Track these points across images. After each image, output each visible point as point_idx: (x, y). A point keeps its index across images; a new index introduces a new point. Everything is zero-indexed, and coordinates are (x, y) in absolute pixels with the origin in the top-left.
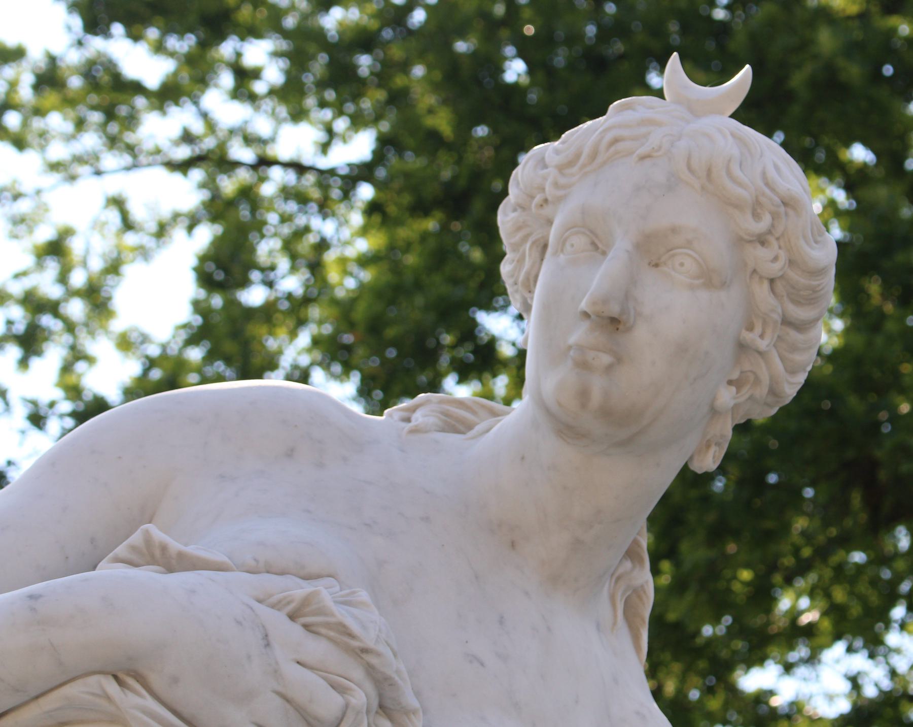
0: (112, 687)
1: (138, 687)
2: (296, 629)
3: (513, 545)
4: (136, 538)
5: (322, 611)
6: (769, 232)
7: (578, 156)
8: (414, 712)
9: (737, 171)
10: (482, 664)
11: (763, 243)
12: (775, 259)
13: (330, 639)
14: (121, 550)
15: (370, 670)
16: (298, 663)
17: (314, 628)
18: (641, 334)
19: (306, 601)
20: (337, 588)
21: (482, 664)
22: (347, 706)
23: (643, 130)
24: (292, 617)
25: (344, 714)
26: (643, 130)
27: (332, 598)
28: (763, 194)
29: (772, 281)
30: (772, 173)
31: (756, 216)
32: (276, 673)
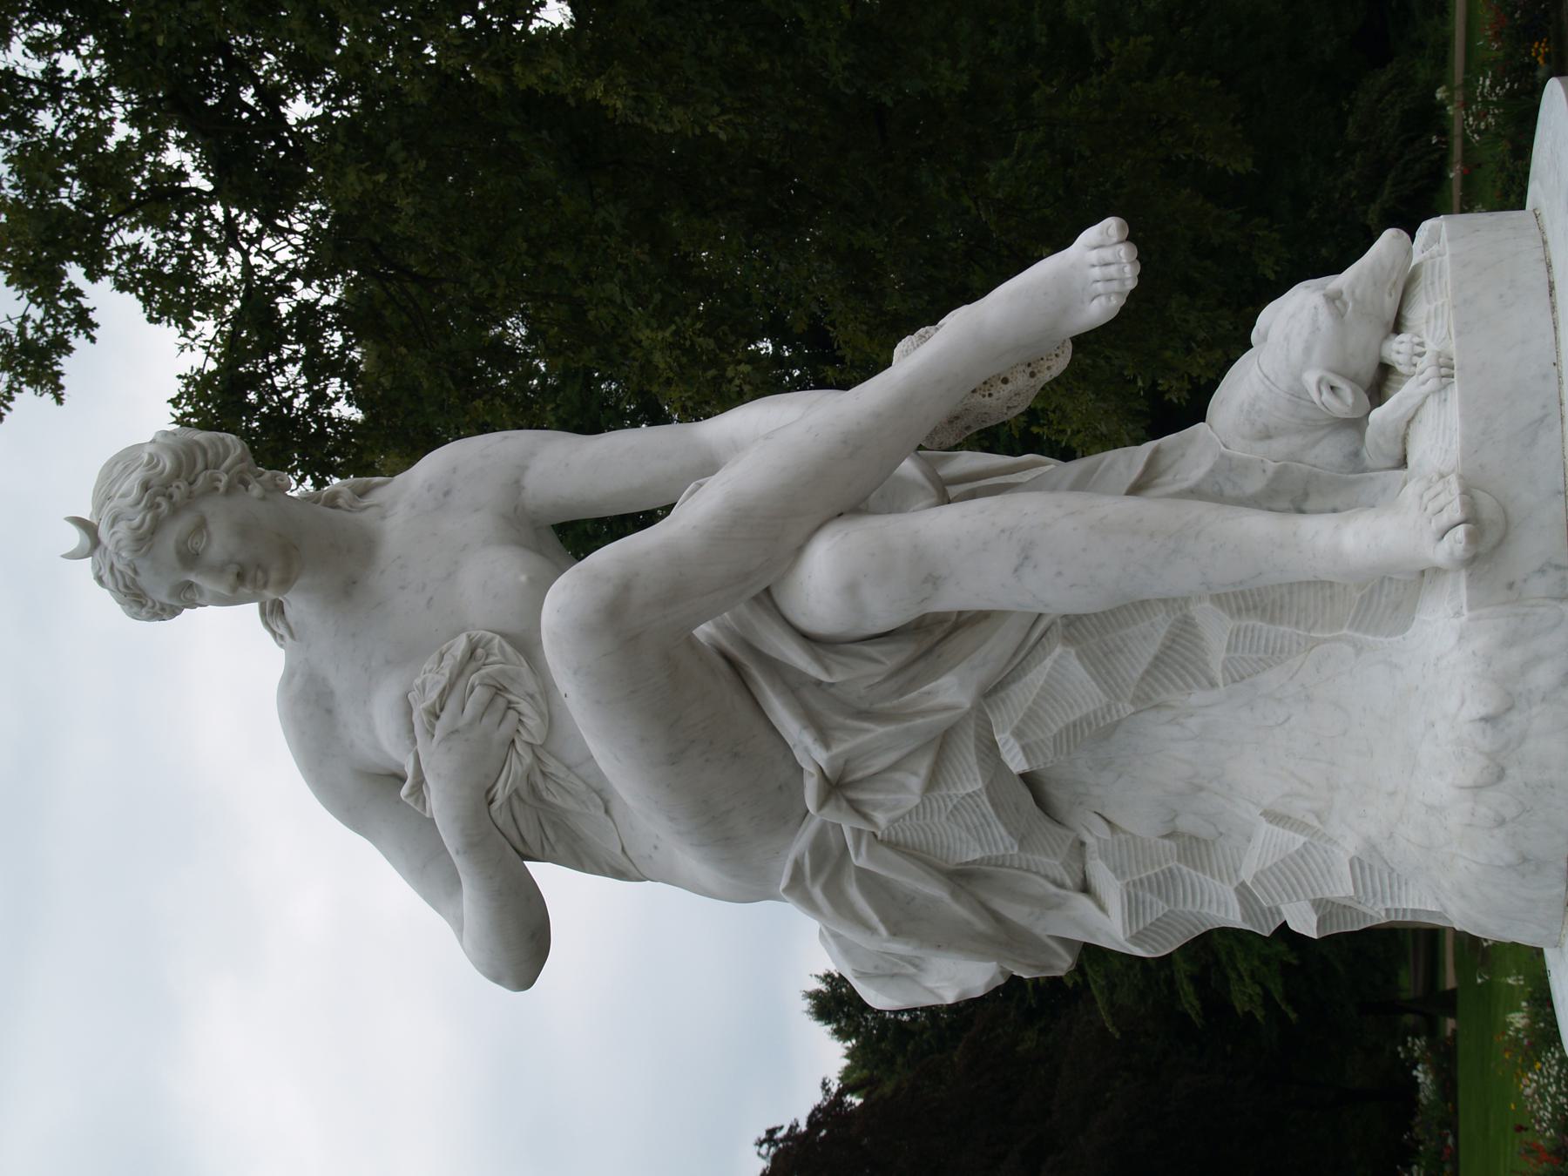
0: (495, 805)
1: (493, 792)
2: (444, 716)
3: (354, 583)
4: (410, 802)
5: (433, 705)
6: (164, 495)
8: (469, 636)
9: (136, 522)
10: (431, 598)
11: (171, 497)
12: (178, 487)
13: (447, 698)
14: (418, 809)
16: (463, 712)
20: (414, 693)
21: (431, 598)
22: (480, 684)
23: (118, 574)
24: (438, 717)
25: (485, 685)
26: (118, 574)
28: (146, 505)
29: (191, 484)
31: (159, 506)
32: (471, 724)
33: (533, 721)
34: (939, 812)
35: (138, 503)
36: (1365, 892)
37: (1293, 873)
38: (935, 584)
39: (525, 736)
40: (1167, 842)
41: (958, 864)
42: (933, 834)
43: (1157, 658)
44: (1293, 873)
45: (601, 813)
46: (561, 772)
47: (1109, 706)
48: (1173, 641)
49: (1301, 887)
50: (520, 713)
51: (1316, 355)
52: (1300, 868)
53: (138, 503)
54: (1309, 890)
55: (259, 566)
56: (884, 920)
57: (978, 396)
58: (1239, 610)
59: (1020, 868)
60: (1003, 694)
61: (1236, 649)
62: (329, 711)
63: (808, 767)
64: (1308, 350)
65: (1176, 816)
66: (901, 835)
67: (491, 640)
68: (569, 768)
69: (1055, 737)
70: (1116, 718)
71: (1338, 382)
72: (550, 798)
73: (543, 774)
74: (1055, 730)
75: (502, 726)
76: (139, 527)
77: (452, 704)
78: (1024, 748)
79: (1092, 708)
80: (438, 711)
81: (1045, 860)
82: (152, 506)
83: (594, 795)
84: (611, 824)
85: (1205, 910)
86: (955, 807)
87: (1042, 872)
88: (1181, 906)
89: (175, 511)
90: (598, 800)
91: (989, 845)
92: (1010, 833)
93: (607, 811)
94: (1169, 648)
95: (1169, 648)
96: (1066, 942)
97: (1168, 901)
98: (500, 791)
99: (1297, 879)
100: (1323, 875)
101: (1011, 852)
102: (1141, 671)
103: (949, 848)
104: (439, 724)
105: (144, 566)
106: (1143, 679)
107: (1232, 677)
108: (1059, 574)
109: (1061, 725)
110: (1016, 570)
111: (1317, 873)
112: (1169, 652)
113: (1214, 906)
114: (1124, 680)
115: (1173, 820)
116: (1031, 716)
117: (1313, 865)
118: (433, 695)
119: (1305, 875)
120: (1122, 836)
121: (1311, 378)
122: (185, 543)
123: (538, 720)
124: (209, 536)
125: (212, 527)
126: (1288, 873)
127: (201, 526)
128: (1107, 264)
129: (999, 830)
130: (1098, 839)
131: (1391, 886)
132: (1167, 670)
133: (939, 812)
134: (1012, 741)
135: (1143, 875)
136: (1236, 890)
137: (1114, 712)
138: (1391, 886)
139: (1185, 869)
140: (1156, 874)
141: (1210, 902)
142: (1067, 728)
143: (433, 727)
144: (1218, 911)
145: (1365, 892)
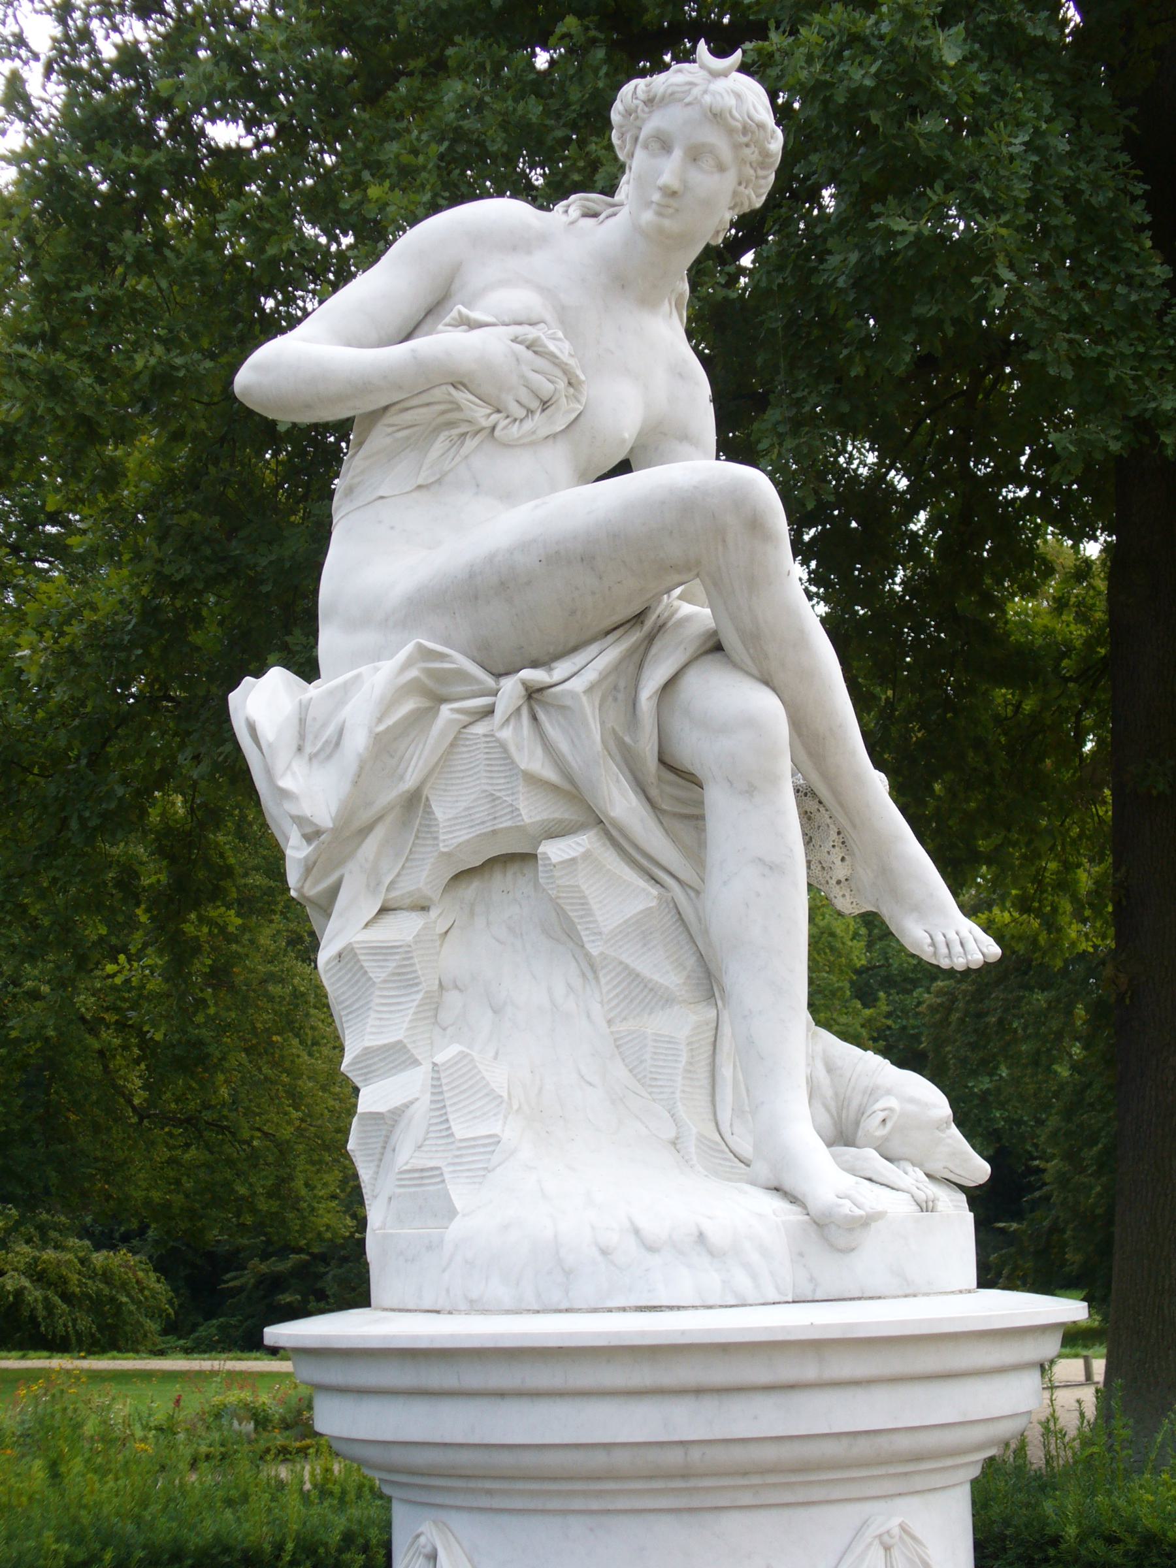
3: (623, 286)
15: (565, 372)
17: (512, 722)
24: (528, 348)
34: (492, 784)
36: (459, 1148)
37: (471, 1087)
38: (747, 792)
40: (437, 982)
41: (427, 799)
42: (463, 778)
43: (638, 975)
44: (471, 1087)
45: (420, 481)
46: (464, 451)
47: (600, 933)
48: (651, 990)
50: (521, 420)
51: (911, 1108)
52: (476, 1092)
53: (752, 120)
54: (455, 1100)
56: (388, 729)
57: (833, 835)
61: (656, 1041)
63: (561, 669)
64: (912, 1100)
65: (461, 991)
66: (465, 749)
67: (579, 401)
69: (578, 886)
71: (889, 1125)
72: (442, 437)
73: (464, 435)
74: (584, 887)
75: (515, 404)
76: (730, 113)
77: (540, 362)
78: (573, 860)
79: (600, 919)
80: (536, 349)
81: (425, 873)
82: (745, 130)
83: (438, 476)
84: (408, 489)
85: (373, 1015)
86: (499, 798)
87: (404, 872)
88: (378, 993)
89: (737, 147)
90: (431, 480)
91: (450, 826)
92: (459, 845)
94: (646, 986)
95: (646, 986)
96: (334, 892)
97: (385, 981)
98: (464, 395)
99: (465, 1091)
100: (470, 1112)
101: (441, 845)
102: (628, 961)
103: (445, 790)
106: (621, 963)
107: (621, 1038)
108: (758, 895)
109: (587, 893)
110: (760, 860)
111: (472, 1108)
112: (642, 985)
113: (377, 1023)
114: (620, 947)
115: (456, 987)
117: (479, 1104)
118: (552, 347)
119: (468, 1097)
120: (438, 943)
121: (892, 1102)
122: (711, 152)
123: (516, 436)
126: (470, 1083)
127: (721, 168)
128: (962, 944)
129: (464, 835)
130: (435, 922)
131: (468, 1170)
132: (625, 984)
133: (492, 784)
134: (582, 850)
135: (416, 960)
136: (400, 1042)
137: (592, 938)
138: (468, 1170)
139: (420, 996)
140: (415, 971)
141: (380, 1019)
142: (584, 897)
143: (520, 343)
144: (373, 1026)
145: (459, 1148)
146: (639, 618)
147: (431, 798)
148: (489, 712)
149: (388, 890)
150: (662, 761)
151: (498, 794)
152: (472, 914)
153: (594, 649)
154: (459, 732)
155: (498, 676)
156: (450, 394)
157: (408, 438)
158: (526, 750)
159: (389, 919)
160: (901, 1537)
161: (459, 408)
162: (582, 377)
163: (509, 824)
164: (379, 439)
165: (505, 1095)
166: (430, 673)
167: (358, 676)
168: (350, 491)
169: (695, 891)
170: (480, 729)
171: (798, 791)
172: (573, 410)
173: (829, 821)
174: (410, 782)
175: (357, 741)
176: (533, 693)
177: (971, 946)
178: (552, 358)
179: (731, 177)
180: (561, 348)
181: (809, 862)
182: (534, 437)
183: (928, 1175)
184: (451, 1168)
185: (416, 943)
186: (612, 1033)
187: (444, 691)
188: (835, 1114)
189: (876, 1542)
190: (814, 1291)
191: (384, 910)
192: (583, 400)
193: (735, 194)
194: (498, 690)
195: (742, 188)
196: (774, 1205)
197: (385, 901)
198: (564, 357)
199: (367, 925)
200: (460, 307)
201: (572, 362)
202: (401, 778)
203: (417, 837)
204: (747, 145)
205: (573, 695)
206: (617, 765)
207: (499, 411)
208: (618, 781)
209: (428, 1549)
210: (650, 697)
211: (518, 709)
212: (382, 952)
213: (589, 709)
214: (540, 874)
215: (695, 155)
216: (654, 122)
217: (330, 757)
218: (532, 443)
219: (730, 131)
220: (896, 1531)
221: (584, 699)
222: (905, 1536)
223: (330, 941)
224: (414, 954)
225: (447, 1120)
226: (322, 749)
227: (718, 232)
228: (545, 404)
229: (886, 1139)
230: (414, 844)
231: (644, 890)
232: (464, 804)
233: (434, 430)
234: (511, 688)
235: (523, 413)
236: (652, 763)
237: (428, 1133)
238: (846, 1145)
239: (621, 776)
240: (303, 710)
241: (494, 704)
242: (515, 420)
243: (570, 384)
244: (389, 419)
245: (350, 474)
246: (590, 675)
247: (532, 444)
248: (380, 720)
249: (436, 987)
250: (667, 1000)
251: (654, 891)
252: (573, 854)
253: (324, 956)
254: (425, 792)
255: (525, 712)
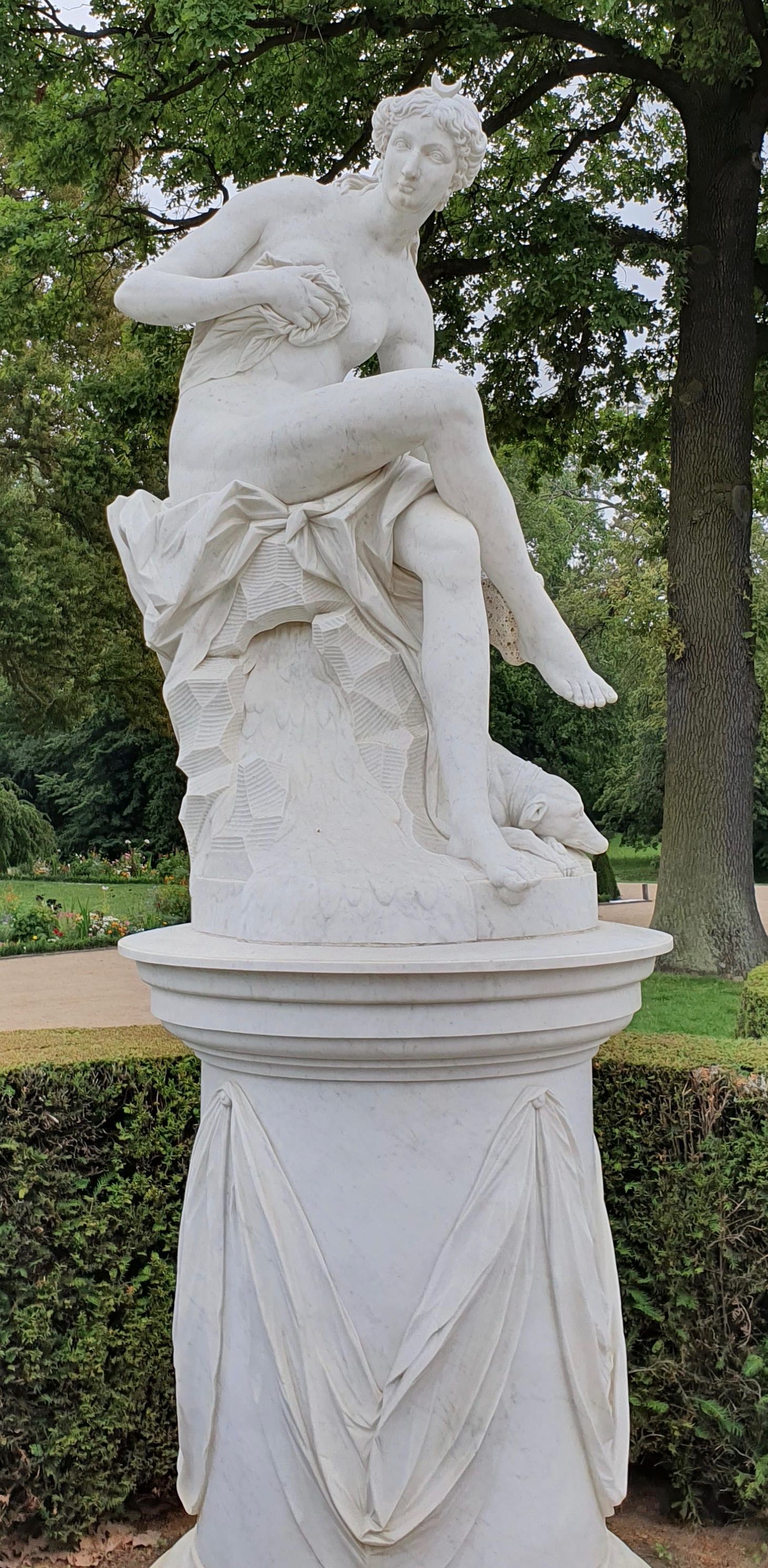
0: (261, 309)
5: (322, 280)
7: (401, 111)
15: (336, 298)
17: (298, 538)
18: (422, 180)
19: (317, 276)
23: (424, 105)
24: (312, 281)
27: (275, 781)
30: (467, 122)
32: (309, 301)
33: (302, 337)
35: (466, 126)
39: (294, 332)
41: (240, 585)
45: (238, 370)
46: (268, 350)
49: (255, 788)
52: (267, 787)
53: (466, 126)
55: (414, 189)
58: (411, 755)
59: (227, 619)
60: (359, 619)
62: (305, 211)
63: (330, 502)
67: (345, 317)
68: (270, 354)
70: (342, 682)
71: (542, 813)
73: (269, 338)
77: (321, 291)
82: (462, 135)
86: (287, 587)
89: (456, 147)
93: (238, 372)
96: (176, 643)
97: (206, 707)
102: (370, 697)
104: (309, 281)
105: (429, 122)
108: (458, 658)
109: (344, 651)
111: (264, 797)
115: (255, 710)
116: (353, 635)
117: (269, 795)
118: (328, 280)
124: (438, 164)
125: (443, 166)
127: (445, 161)
134: (342, 624)
136: (217, 747)
143: (308, 278)
146: (383, 469)
147: (242, 585)
148: (282, 529)
149: (212, 644)
150: (394, 563)
151: (287, 584)
152: (267, 661)
153: (353, 489)
154: (262, 542)
155: (288, 504)
156: (259, 312)
157: (232, 339)
158: (306, 556)
159: (213, 663)
160: (547, 1102)
161: (266, 321)
162: (348, 301)
163: (294, 604)
164: (211, 339)
165: (287, 790)
166: (243, 501)
167: (196, 501)
168: (190, 374)
169: (414, 650)
170: (276, 540)
171: (483, 584)
172: (341, 323)
173: (503, 604)
174: (227, 576)
175: (194, 548)
176: (311, 519)
177: (598, 692)
178: (328, 288)
179: (453, 165)
180: (335, 283)
181: (490, 630)
182: (315, 341)
183: (566, 846)
184: (250, 839)
185: (229, 681)
186: (359, 745)
187: (250, 514)
188: (505, 803)
189: (530, 1105)
190: (491, 933)
191: (208, 657)
192: (348, 317)
193: (454, 178)
194: (289, 515)
195: (458, 174)
196: (465, 870)
197: (209, 651)
198: (336, 288)
199: (197, 667)
200: (267, 252)
201: (341, 291)
202: (223, 571)
203: (232, 610)
204: (464, 145)
205: (339, 522)
206: (367, 568)
207: (292, 323)
208: (366, 578)
209: (226, 1102)
210: (389, 524)
211: (302, 530)
212: (206, 686)
213: (348, 529)
214: (314, 638)
215: (427, 150)
216: (403, 127)
217: (174, 556)
218: (313, 345)
219: (452, 135)
220: (543, 1098)
221: (345, 524)
222: (549, 1100)
223: (172, 678)
224: (229, 693)
225: (247, 805)
226: (170, 550)
227: (440, 204)
228: (323, 320)
229: (540, 822)
230: (230, 614)
231: (381, 650)
232: (264, 590)
233: (249, 334)
234: (296, 514)
235: (308, 325)
236: (389, 566)
237: (234, 812)
238: (512, 826)
239: (368, 575)
240: (158, 523)
241: (285, 524)
242: (303, 330)
243: (340, 306)
244: (218, 326)
245: (193, 361)
246: (349, 509)
247: (315, 345)
248: (210, 533)
249: (242, 710)
250: (395, 725)
251: (389, 653)
252: (336, 627)
253: (167, 690)
254: (239, 581)
255: (306, 531)
